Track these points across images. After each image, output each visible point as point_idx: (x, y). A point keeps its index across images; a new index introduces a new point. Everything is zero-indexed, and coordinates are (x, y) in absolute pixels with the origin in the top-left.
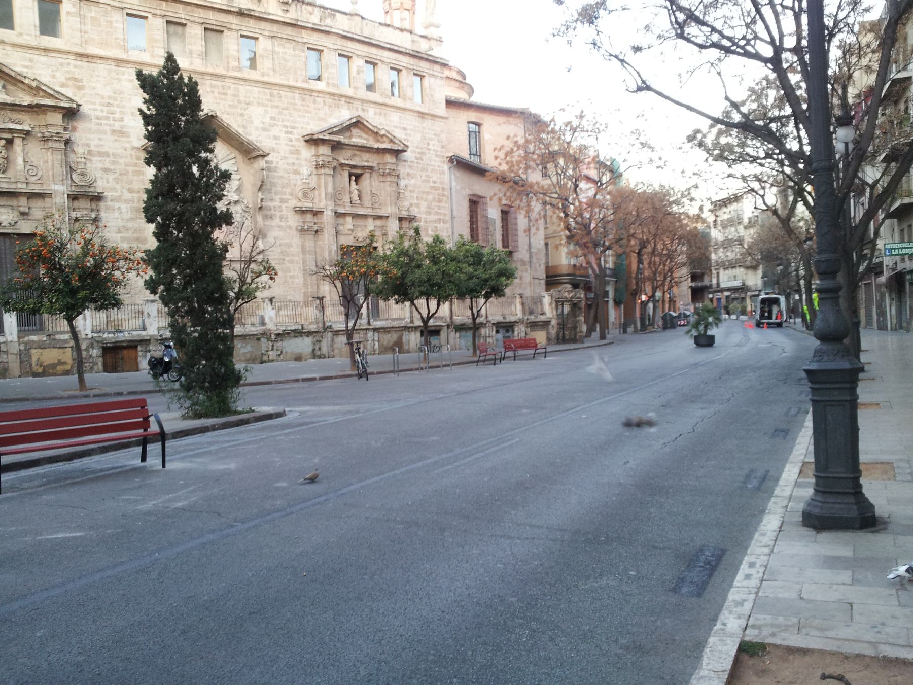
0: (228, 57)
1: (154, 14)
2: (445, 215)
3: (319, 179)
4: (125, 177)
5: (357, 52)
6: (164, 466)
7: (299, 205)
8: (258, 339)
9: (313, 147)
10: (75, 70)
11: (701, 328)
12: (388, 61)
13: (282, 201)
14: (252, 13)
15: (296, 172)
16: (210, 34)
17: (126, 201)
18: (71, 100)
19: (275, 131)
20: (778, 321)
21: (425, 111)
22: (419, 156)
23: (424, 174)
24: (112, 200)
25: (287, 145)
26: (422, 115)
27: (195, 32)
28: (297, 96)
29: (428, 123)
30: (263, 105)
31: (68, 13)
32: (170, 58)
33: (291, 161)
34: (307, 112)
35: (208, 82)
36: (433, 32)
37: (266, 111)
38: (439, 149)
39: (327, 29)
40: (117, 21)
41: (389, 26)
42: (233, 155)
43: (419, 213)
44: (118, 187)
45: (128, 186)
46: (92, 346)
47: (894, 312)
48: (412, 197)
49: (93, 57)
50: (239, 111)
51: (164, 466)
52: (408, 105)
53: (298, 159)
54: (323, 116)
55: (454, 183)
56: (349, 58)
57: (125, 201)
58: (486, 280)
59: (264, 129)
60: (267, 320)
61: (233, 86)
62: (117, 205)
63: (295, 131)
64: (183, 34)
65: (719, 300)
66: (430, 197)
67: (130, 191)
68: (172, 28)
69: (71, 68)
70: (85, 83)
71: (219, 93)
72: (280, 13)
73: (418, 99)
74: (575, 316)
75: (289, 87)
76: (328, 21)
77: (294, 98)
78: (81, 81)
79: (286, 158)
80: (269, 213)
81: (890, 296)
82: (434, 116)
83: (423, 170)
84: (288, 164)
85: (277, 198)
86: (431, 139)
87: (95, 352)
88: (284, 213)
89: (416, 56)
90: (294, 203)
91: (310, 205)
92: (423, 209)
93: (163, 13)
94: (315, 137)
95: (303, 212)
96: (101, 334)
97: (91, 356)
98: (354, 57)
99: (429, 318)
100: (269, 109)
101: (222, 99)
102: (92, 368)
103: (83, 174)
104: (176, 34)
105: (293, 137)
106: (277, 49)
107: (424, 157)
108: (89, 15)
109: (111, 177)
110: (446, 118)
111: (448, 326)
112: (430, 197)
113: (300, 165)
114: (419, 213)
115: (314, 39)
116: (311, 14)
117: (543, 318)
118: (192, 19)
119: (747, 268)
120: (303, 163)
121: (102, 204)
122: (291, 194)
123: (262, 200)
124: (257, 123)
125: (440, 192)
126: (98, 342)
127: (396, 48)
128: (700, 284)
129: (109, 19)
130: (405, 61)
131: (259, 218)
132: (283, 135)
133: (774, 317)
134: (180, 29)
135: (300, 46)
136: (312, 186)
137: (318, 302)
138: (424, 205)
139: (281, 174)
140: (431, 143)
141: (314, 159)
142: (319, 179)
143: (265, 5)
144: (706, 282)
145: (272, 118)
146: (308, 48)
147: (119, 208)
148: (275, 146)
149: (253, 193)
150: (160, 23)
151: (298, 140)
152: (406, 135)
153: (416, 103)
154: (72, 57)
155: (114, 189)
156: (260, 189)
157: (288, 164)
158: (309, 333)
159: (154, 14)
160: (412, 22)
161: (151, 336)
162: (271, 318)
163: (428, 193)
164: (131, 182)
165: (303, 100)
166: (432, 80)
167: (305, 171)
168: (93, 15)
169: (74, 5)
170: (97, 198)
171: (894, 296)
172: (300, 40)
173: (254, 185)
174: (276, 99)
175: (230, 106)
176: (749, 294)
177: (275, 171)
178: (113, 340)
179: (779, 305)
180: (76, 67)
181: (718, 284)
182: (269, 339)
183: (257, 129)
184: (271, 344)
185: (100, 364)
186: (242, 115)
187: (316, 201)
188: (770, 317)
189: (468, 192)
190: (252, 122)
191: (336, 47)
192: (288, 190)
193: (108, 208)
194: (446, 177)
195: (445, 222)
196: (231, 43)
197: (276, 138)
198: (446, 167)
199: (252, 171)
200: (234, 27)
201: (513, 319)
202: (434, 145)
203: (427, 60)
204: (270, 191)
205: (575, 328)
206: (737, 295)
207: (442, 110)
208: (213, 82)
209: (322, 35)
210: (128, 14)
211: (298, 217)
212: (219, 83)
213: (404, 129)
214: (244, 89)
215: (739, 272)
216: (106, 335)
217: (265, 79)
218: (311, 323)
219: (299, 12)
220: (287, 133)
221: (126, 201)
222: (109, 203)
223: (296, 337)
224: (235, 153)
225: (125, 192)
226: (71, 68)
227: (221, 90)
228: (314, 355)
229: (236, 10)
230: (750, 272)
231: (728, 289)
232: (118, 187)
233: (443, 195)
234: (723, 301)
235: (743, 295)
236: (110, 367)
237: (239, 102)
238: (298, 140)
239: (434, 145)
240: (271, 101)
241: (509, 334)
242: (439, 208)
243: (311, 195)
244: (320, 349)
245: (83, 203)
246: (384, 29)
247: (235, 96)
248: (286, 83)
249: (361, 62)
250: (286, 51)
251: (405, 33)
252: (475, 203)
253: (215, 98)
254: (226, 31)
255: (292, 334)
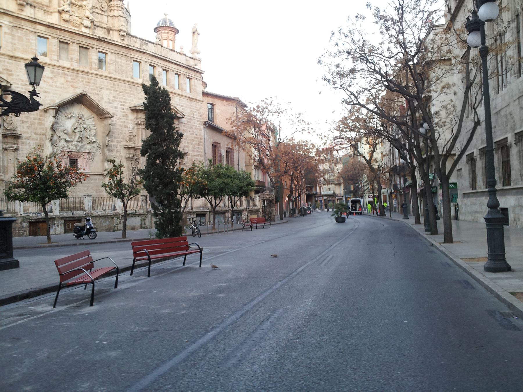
0: (91, 63)
1: (53, 37)
2: (201, 152)
3: (138, 131)
4: (33, 126)
5: (159, 64)
6: (200, 266)
7: (127, 144)
8: (113, 218)
9: (135, 114)
10: (8, 65)
11: (339, 213)
12: (174, 70)
13: (118, 142)
14: (105, 40)
15: (126, 127)
16: (82, 49)
17: (33, 139)
18: (8, 82)
19: (115, 104)
20: (360, 211)
21: (192, 97)
22: (188, 120)
23: (191, 130)
24: (25, 139)
25: (121, 111)
26: (190, 99)
27: (74, 48)
28: (127, 85)
29: (193, 103)
30: (109, 89)
31: (5, 33)
32: (153, 79)
33: (123, 120)
34: (132, 94)
35: (80, 76)
36: (196, 56)
37: (110, 93)
38: (199, 117)
39: (144, 51)
40: (32, 39)
41: (174, 51)
42: (92, 116)
43: (189, 150)
44: (29, 131)
45: (35, 131)
46: (23, 221)
47: (422, 207)
48: (185, 142)
49: (18, 58)
50: (96, 92)
51: (200, 266)
52: (184, 94)
53: (127, 119)
54: (140, 97)
55: (206, 136)
56: (154, 67)
57: (33, 139)
58: (242, 188)
59: (110, 103)
60: (117, 207)
61: (94, 78)
62: (28, 141)
63: (126, 104)
64: (67, 49)
65: (321, 201)
66: (194, 142)
67: (36, 134)
68: (62, 45)
69: (6, 64)
70: (13, 73)
71: (86, 82)
72: (120, 41)
73: (188, 91)
74: (270, 207)
75: (123, 80)
76: (144, 47)
77: (126, 87)
78: (11, 71)
79: (120, 119)
80: (110, 148)
81: (420, 199)
82: (197, 100)
83: (191, 128)
84: (122, 122)
85: (115, 140)
86: (195, 112)
87: (25, 224)
88: (119, 148)
89: (188, 68)
90: (124, 143)
91: (133, 145)
92: (190, 149)
93: (58, 37)
94: (138, 108)
95: (129, 148)
96: (28, 214)
97: (23, 227)
98: (157, 67)
99: (216, 206)
100: (112, 92)
101: (87, 85)
102: (23, 233)
103: (10, 123)
104: (63, 48)
105: (124, 107)
106: (117, 60)
107: (191, 121)
108: (17, 35)
109: (25, 125)
110: (202, 101)
111: (210, 212)
112: (194, 142)
113: (128, 123)
114: (189, 150)
115: (137, 56)
116: (135, 42)
117: (256, 208)
118: (73, 41)
119: (336, 184)
120: (130, 121)
121: (20, 141)
122: (123, 139)
123: (109, 141)
124: (106, 99)
125: (199, 140)
126: (27, 219)
127: (178, 63)
128: (310, 193)
129: (28, 38)
130: (182, 70)
131: (106, 151)
132: (119, 106)
133: (357, 209)
134: (65, 46)
135: (129, 59)
136: (134, 134)
137: (144, 198)
138: (191, 146)
139: (118, 127)
140: (195, 114)
141: (136, 120)
142: (138, 131)
143: (112, 36)
144: (314, 192)
145: (114, 97)
146: (134, 61)
147: (29, 143)
148: (115, 112)
149: (103, 137)
150: (56, 42)
151: (127, 109)
152: (183, 109)
153: (187, 93)
154: (6, 57)
155: (27, 133)
156: (107, 135)
157: (122, 122)
158: (139, 215)
159: (53, 37)
160: (174, 46)
161: (56, 216)
162: (119, 206)
163: (193, 140)
164: (36, 129)
165: (130, 88)
166: (196, 81)
167: (131, 126)
168: (19, 35)
169: (9, 29)
170: (17, 137)
171: (422, 199)
172: (129, 56)
173: (103, 133)
174: (116, 87)
175: (92, 89)
176: (337, 198)
177: (115, 126)
178: (35, 218)
179: (360, 204)
180: (8, 63)
181: (320, 192)
182: (118, 218)
183: (106, 102)
184: (119, 220)
185: (28, 231)
186: (98, 94)
187: (136, 142)
188: (356, 210)
189: (212, 140)
190: (103, 98)
191: (148, 61)
192: (121, 136)
193: (23, 143)
194: (202, 132)
195: (201, 156)
196: (94, 56)
197: (115, 107)
198: (202, 127)
199: (103, 125)
200: (95, 47)
201: (241, 208)
202: (196, 115)
203: (193, 70)
204: (111, 137)
205: (271, 213)
206: (330, 199)
207: (200, 97)
208: (83, 76)
209: (141, 54)
210: (39, 36)
211: (126, 151)
212: (86, 77)
213: (182, 106)
214: (99, 80)
215: (332, 186)
216: (31, 215)
217: (111, 75)
218: (140, 209)
219: (129, 42)
220: (121, 105)
221: (33, 139)
222: (24, 140)
223: (132, 217)
224: (94, 115)
225: (33, 134)
226: (6, 64)
227: (87, 80)
228: (141, 227)
229: (97, 38)
230: (337, 187)
231: (326, 195)
232: (29, 131)
233: (201, 142)
234: (323, 201)
235: (333, 199)
236: (33, 233)
237: (97, 87)
238: (127, 109)
239: (196, 115)
240: (113, 87)
241: (239, 216)
242: (199, 148)
243: (133, 139)
244: (145, 223)
245: (10, 140)
246: (172, 52)
247: (95, 84)
248: (121, 78)
249: (160, 70)
250: (122, 61)
251: (183, 56)
252: (215, 146)
253: (84, 85)
254: (91, 48)
255: (130, 216)
